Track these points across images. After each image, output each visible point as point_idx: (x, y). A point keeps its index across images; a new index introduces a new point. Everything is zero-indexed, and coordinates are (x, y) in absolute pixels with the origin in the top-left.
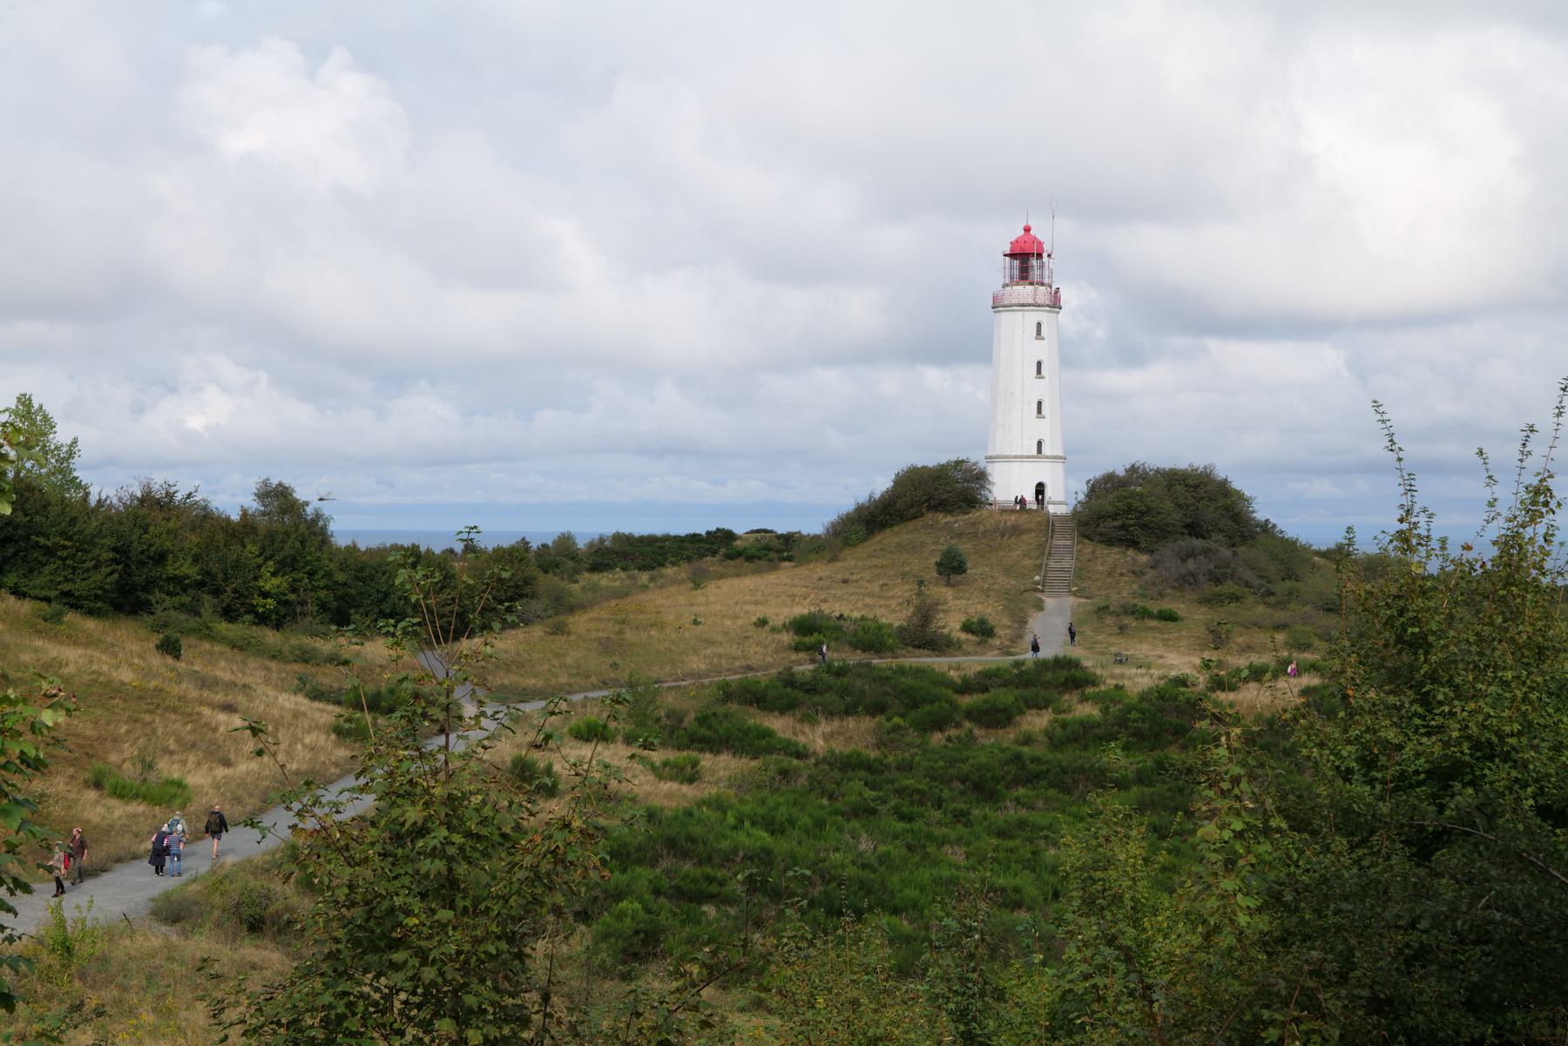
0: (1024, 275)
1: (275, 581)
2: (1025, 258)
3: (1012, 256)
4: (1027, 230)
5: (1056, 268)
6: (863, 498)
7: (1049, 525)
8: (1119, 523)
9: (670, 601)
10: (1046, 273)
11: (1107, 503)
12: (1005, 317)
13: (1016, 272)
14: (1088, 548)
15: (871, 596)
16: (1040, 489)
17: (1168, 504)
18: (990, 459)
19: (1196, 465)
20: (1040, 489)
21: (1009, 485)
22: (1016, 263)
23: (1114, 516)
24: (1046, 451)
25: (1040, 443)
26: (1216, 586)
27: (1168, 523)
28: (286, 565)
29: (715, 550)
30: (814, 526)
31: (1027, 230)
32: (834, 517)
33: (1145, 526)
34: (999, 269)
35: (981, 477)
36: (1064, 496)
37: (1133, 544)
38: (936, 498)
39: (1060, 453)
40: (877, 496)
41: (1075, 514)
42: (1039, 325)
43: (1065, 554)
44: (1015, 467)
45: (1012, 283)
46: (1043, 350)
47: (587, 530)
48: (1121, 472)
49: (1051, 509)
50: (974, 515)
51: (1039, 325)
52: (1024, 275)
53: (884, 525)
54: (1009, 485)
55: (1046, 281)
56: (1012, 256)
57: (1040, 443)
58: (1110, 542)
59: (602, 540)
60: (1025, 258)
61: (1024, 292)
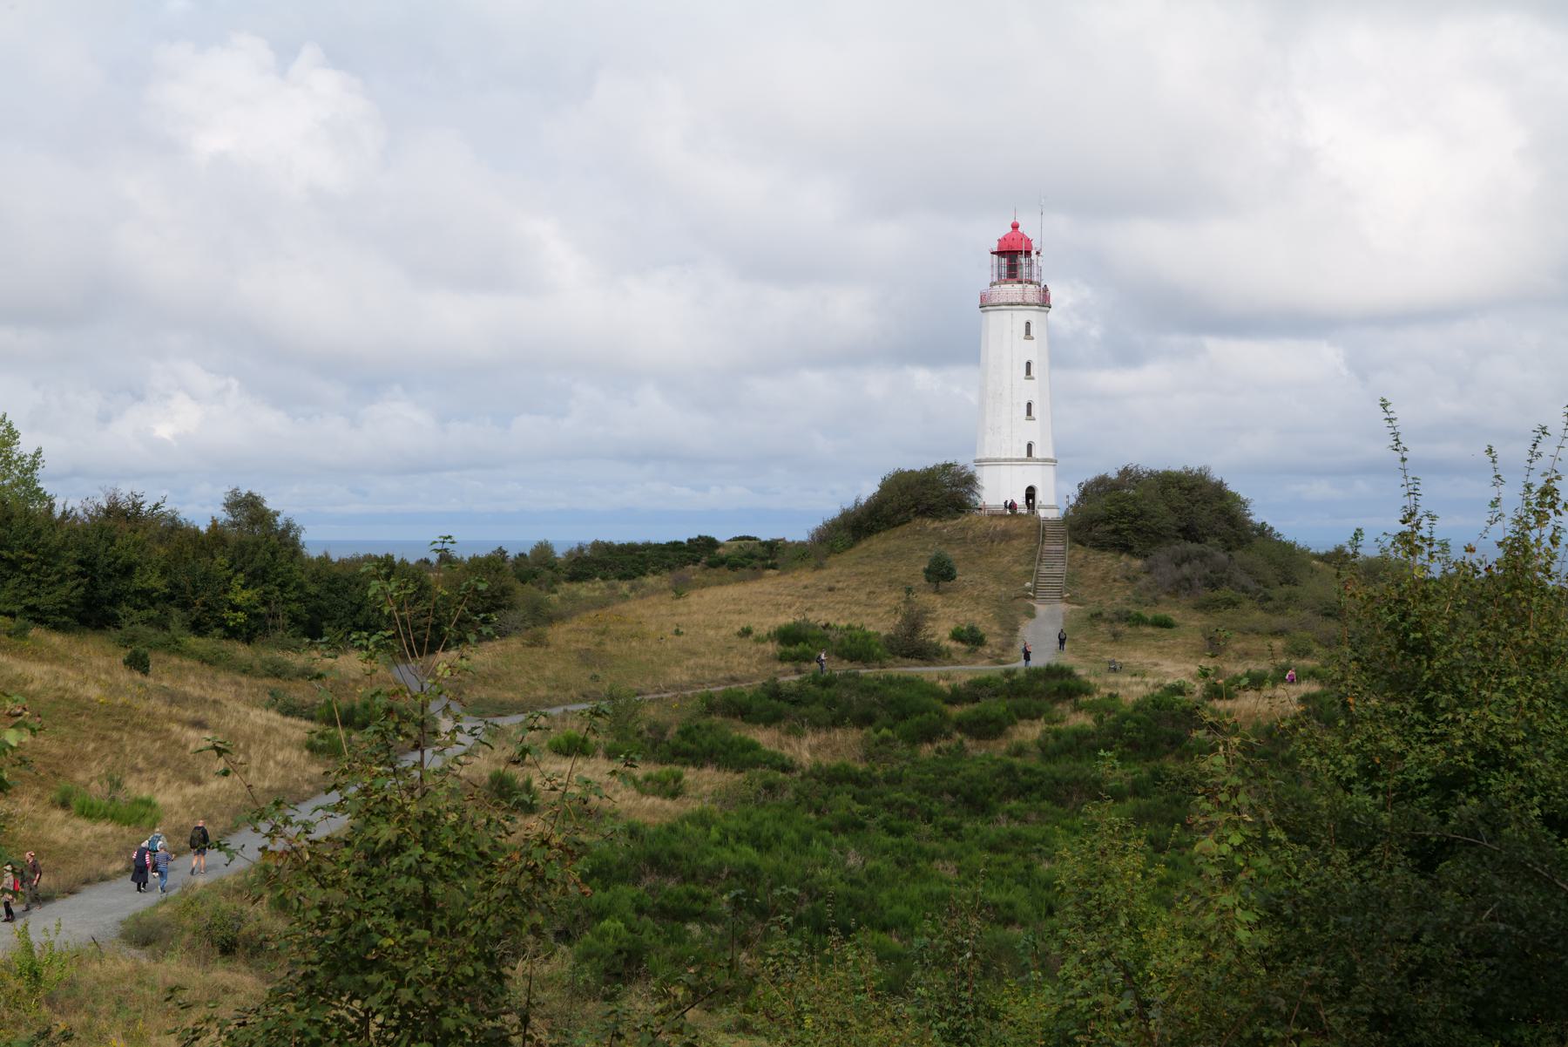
0: (1012, 274)
1: (246, 594)
2: (1013, 255)
3: (1000, 253)
4: (1015, 227)
5: (1044, 265)
6: (849, 504)
7: (1040, 531)
8: (1112, 527)
9: (651, 610)
10: (1035, 271)
11: (1099, 507)
12: (993, 317)
13: (1004, 270)
14: (1081, 552)
15: (858, 604)
16: (1030, 493)
17: (1162, 508)
18: (980, 462)
19: (1190, 467)
20: (1030, 493)
21: (998, 489)
22: (1004, 261)
23: (1107, 520)
24: (1036, 453)
25: (1030, 446)
26: (1212, 591)
27: (1166, 529)
28: (257, 577)
29: (697, 559)
30: (798, 533)
31: (1015, 227)
32: (819, 524)
33: (1138, 531)
34: (987, 267)
35: (970, 481)
36: (1055, 501)
37: (1126, 548)
38: (925, 502)
39: (1051, 456)
40: (863, 501)
41: (1066, 519)
42: (1028, 324)
43: (1057, 560)
44: (1005, 471)
45: (1000, 282)
46: (1033, 351)
47: (566, 538)
48: (1113, 475)
49: (1042, 513)
50: (963, 520)
51: (1028, 324)
52: (1012, 274)
53: (870, 532)
54: (998, 489)
55: (1035, 279)
56: (1000, 253)
57: (1030, 446)
58: (1101, 546)
59: (581, 549)
60: (1013, 255)
61: (1012, 290)
